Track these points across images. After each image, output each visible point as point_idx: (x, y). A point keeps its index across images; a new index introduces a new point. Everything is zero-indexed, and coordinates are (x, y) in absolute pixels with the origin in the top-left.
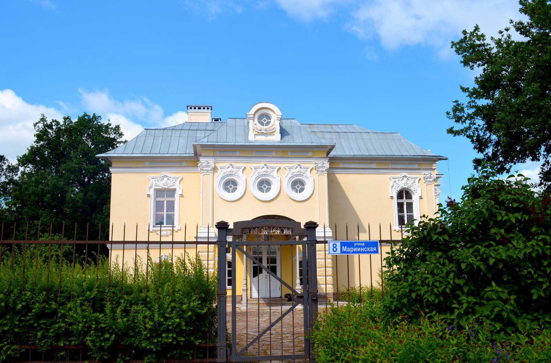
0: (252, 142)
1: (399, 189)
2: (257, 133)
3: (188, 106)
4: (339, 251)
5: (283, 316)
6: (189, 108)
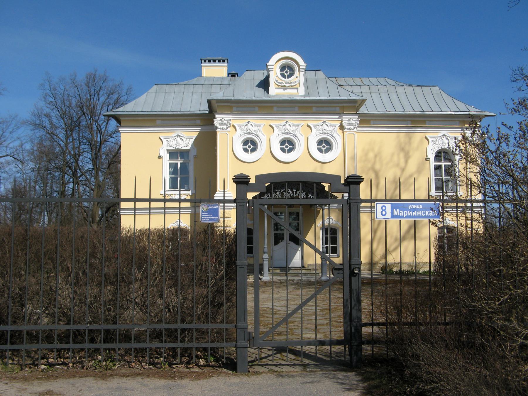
0: (273, 96)
1: (437, 149)
2: (277, 86)
3: (201, 60)
4: (388, 215)
5: (303, 304)
6: (203, 61)
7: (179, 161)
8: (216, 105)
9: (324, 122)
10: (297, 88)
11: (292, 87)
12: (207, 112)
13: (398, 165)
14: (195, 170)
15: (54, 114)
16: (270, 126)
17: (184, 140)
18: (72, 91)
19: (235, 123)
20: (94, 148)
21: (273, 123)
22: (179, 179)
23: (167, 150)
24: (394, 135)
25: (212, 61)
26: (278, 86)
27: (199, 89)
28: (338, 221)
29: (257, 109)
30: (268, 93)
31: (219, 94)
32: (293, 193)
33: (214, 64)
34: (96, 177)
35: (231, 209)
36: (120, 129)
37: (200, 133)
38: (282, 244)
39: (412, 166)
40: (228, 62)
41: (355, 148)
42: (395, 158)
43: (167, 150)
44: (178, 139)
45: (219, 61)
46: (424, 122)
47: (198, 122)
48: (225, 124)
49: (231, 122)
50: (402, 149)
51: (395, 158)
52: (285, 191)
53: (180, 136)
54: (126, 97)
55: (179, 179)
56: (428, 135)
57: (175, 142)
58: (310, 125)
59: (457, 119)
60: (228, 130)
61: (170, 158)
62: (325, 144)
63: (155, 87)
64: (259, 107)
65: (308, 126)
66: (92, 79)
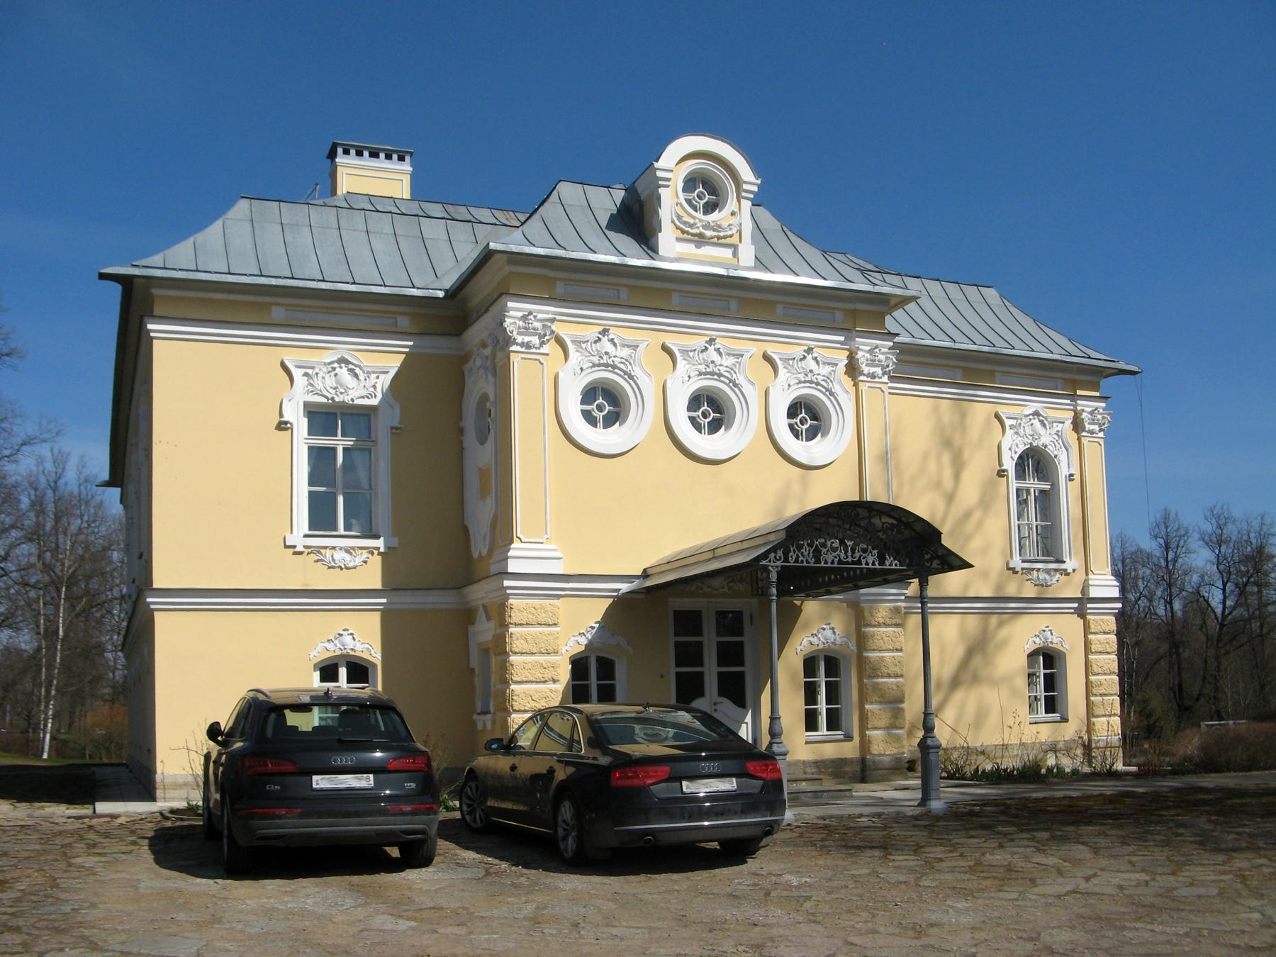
1: (1021, 449)
2: (681, 236)
6: (340, 150)
7: (340, 443)
11: (719, 242)
13: (938, 485)
14: (426, 475)
17: (362, 377)
22: (341, 499)
23: (306, 405)
25: (366, 153)
26: (683, 232)
28: (847, 636)
29: (624, 294)
32: (846, 552)
33: (374, 163)
35: (559, 597)
36: (150, 326)
37: (410, 359)
42: (932, 466)
43: (306, 405)
44: (343, 372)
46: (991, 375)
47: (404, 322)
48: (535, 332)
49: (554, 328)
50: (947, 443)
51: (932, 466)
52: (824, 545)
53: (347, 362)
55: (341, 499)
56: (1003, 411)
57: (330, 381)
58: (774, 356)
59: (1059, 375)
60: (542, 350)
62: (808, 415)
63: (243, 205)
64: (632, 289)
65: (766, 357)
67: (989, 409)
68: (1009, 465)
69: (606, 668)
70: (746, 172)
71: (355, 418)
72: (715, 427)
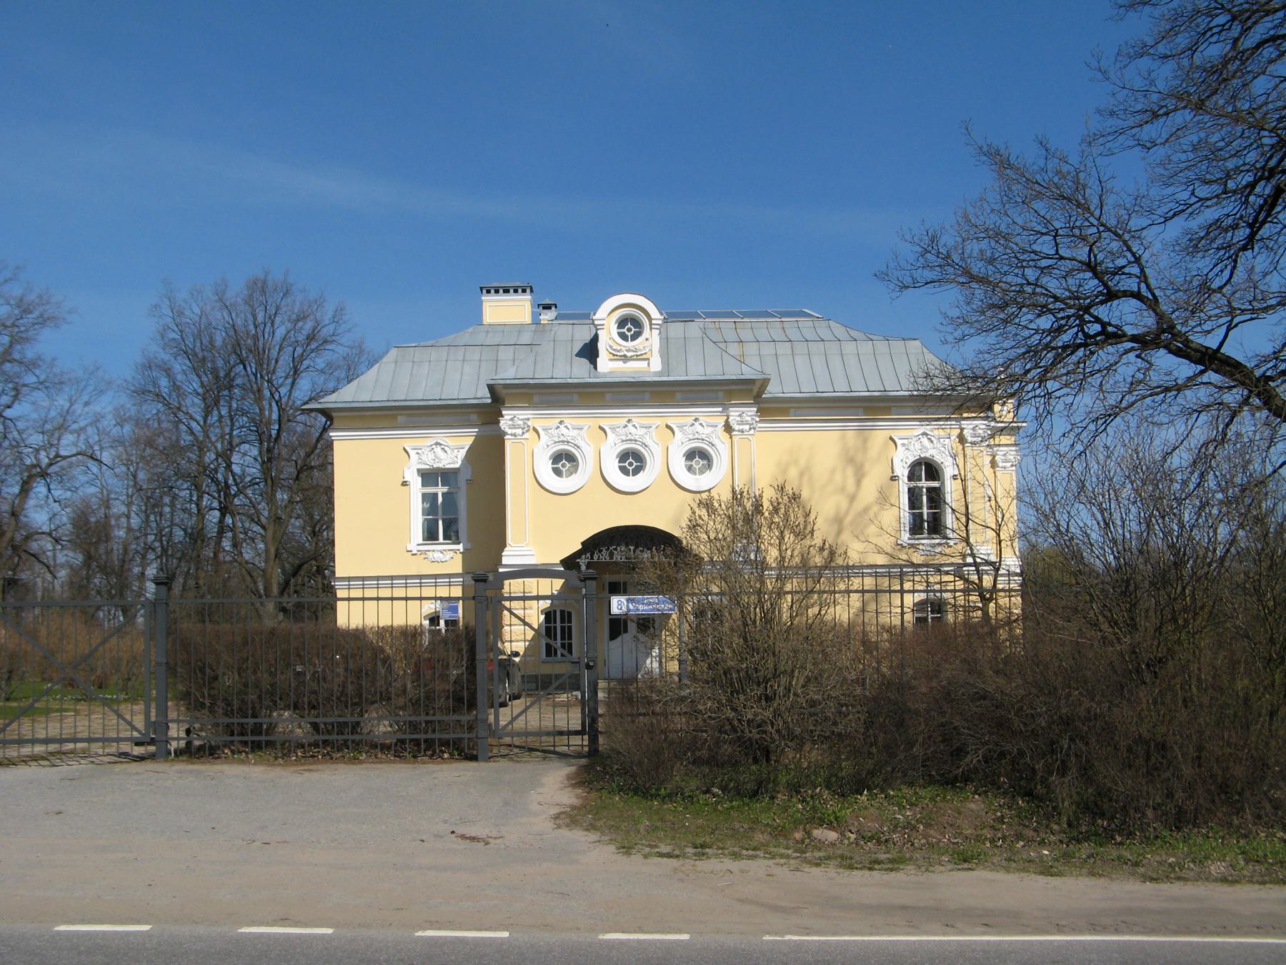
0: (605, 375)
1: (911, 460)
7: (440, 490)
8: (504, 392)
9: (696, 420)
10: (647, 358)
11: (638, 358)
12: (489, 401)
13: (843, 489)
14: (468, 507)
15: (180, 366)
16: (601, 428)
18: (219, 317)
19: (539, 424)
20: (265, 437)
21: (605, 423)
24: (835, 435)
27: (474, 354)
29: (576, 397)
30: (596, 368)
31: (509, 374)
33: (506, 297)
34: (271, 500)
38: (626, 638)
39: (869, 492)
40: (532, 291)
41: (752, 465)
42: (838, 477)
44: (438, 449)
45: (516, 291)
46: (887, 410)
47: (474, 417)
50: (850, 460)
54: (332, 328)
55: (440, 522)
57: (431, 456)
61: (425, 484)
64: (580, 394)
65: (668, 427)
66: (259, 287)
67: (887, 434)
68: (902, 472)
69: (566, 616)
70: (654, 313)
71: (446, 476)
72: (637, 471)
